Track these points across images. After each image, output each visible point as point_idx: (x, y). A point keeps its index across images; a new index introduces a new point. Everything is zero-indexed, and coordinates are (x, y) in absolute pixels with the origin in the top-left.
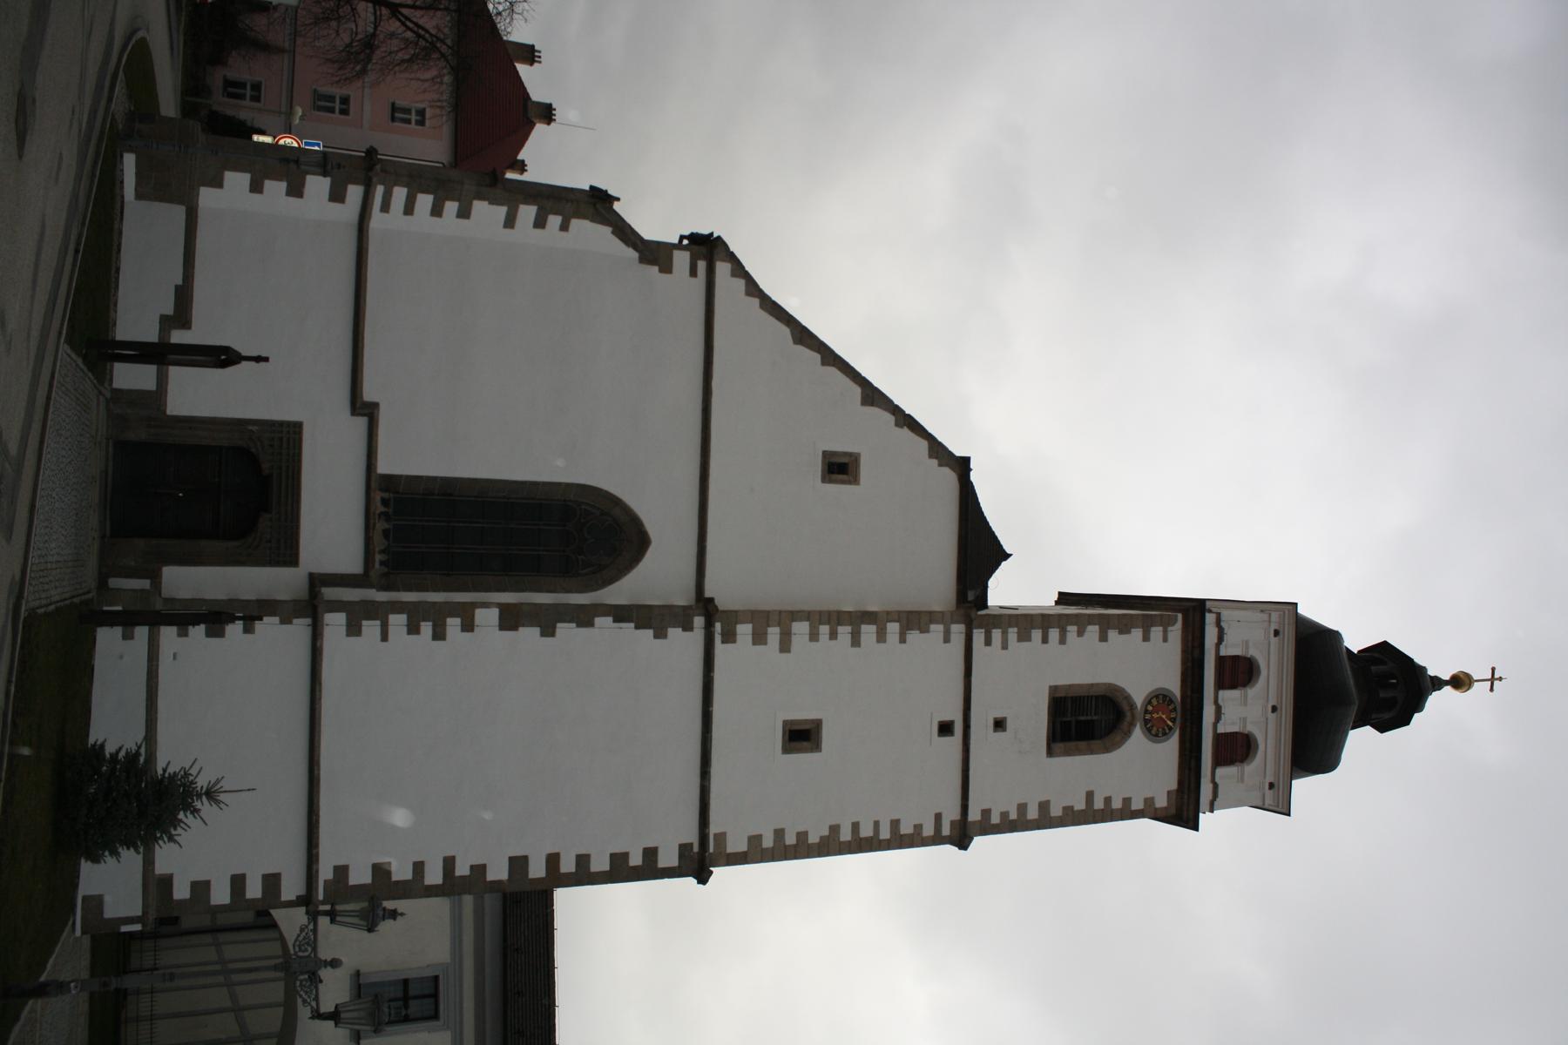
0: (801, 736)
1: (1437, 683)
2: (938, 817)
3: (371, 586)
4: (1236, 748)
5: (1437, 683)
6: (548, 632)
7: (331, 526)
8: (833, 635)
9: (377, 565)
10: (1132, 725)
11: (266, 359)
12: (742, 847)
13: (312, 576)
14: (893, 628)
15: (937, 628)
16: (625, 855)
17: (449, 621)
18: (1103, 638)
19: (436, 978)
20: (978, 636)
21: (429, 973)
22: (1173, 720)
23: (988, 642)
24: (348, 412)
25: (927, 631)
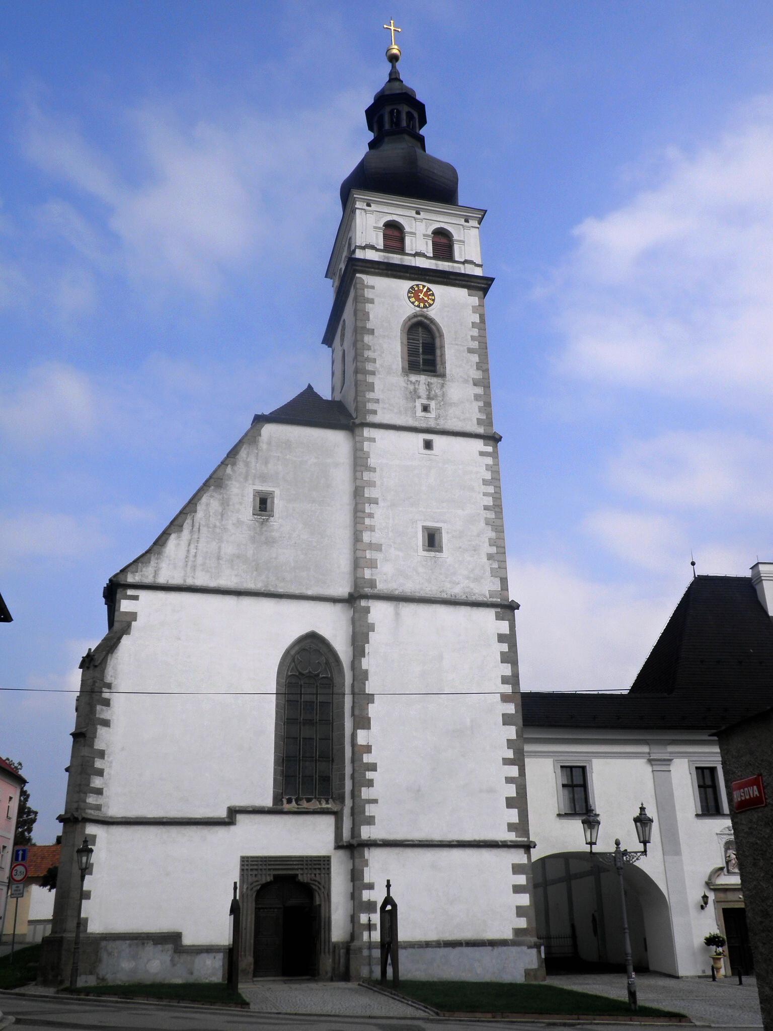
0: (432, 540)
1: (394, 77)
2: (482, 454)
3: (342, 810)
4: (443, 244)
5: (394, 77)
6: (370, 698)
7: (306, 837)
8: (371, 516)
9: (329, 806)
10: (426, 317)
11: (388, 881)
12: (498, 581)
13: (338, 847)
14: (366, 476)
16: (502, 653)
17: (365, 760)
19: (562, 767)
20: (371, 419)
21: (559, 770)
22: (424, 286)
24: (232, 828)
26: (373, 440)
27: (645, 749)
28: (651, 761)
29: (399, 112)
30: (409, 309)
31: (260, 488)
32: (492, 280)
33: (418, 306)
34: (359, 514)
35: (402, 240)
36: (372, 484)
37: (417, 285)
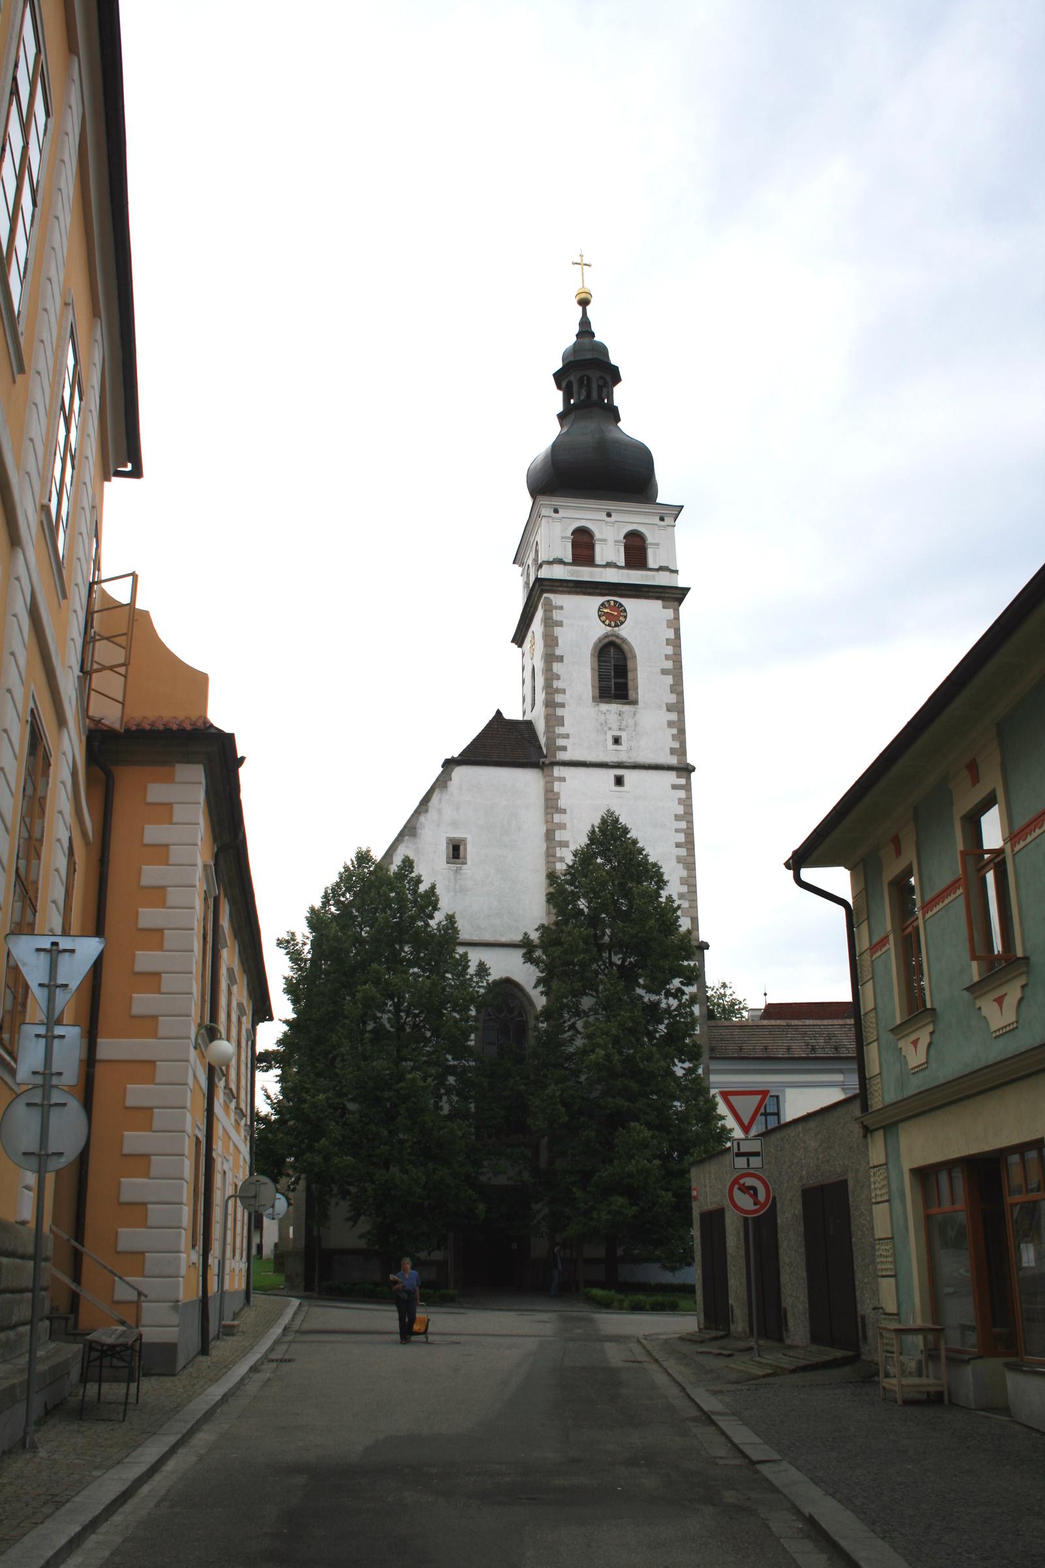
1: (585, 330)
2: (675, 787)
5: (585, 330)
10: (618, 637)
15: (557, 786)
18: (560, 659)
20: (562, 756)
23: (564, 749)
25: (558, 793)
26: (563, 779)
27: (839, 1077)
29: (589, 379)
30: (599, 630)
32: (688, 589)
33: (609, 625)
35: (592, 547)
36: (562, 826)
37: (608, 601)
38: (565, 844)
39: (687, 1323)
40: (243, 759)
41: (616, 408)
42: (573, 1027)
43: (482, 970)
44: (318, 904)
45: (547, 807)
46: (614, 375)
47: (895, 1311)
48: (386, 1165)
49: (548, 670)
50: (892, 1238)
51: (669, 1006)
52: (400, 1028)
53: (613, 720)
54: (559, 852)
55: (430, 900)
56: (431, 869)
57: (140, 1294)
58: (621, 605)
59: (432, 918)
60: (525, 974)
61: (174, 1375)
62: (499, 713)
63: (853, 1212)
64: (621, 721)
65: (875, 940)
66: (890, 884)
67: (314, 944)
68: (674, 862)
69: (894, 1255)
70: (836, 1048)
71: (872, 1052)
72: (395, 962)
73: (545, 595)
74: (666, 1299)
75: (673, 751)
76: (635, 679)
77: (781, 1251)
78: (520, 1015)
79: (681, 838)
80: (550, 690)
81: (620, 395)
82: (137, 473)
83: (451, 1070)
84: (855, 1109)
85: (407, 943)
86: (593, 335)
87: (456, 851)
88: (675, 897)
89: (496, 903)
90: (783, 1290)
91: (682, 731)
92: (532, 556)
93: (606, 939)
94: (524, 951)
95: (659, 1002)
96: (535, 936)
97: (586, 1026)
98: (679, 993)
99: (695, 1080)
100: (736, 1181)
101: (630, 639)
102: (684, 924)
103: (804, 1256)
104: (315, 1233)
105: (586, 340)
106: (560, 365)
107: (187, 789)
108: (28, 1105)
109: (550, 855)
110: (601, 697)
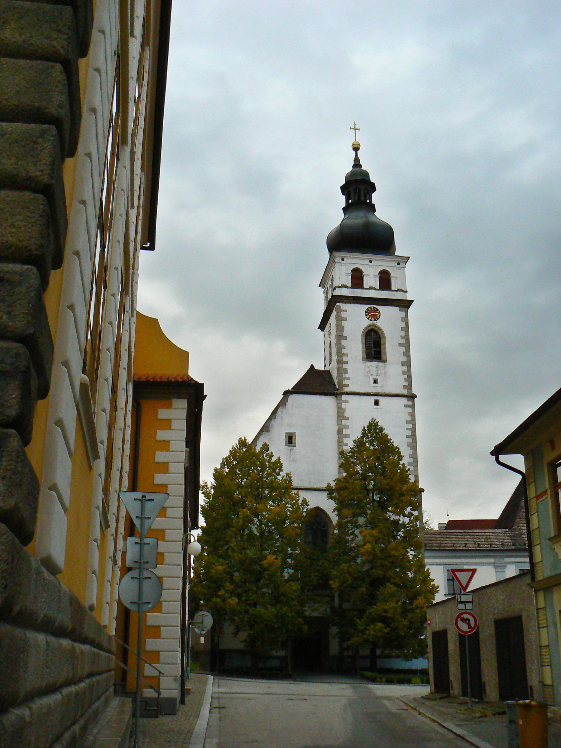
1: (357, 164)
2: (406, 406)
4: (385, 280)
5: (357, 164)
10: (375, 326)
15: (344, 406)
18: (345, 338)
20: (346, 389)
23: (348, 385)
25: (345, 409)
26: (347, 402)
27: (492, 560)
28: (495, 567)
29: (359, 190)
30: (366, 323)
31: (288, 431)
32: (413, 301)
33: (371, 320)
34: (341, 444)
35: (361, 279)
36: (347, 427)
37: (371, 307)
38: (348, 436)
39: (426, 690)
40: (206, 396)
41: (374, 205)
42: (353, 533)
43: (305, 502)
44: (219, 467)
45: (338, 416)
46: (372, 188)
47: (551, 684)
48: (255, 605)
49: (339, 344)
50: (548, 646)
51: (404, 522)
52: (262, 534)
53: (373, 370)
54: (345, 440)
55: (278, 465)
56: (278, 449)
57: (160, 673)
58: (377, 310)
59: (279, 474)
60: (328, 506)
61: (175, 714)
62: (312, 366)
63: (526, 633)
64: (377, 371)
65: (539, 493)
66: (548, 464)
67: (215, 488)
68: (406, 446)
69: (550, 654)
70: (491, 545)
71: (537, 550)
72: (259, 498)
73: (337, 304)
74: (404, 677)
75: (405, 387)
76: (385, 349)
77: (482, 652)
78: (324, 526)
79: (409, 433)
80: (339, 355)
81: (376, 198)
82: (152, 248)
83: (290, 556)
84: (528, 579)
85: (266, 488)
86: (361, 166)
87: (290, 439)
88: (406, 464)
89: (312, 467)
90: (482, 672)
91: (410, 376)
92: (330, 283)
93: (371, 486)
94: (328, 493)
95: (399, 520)
96: (333, 484)
97: (361, 532)
98: (409, 515)
99: (418, 560)
100: (459, 616)
101: (382, 328)
102: (412, 479)
103: (496, 656)
104: (216, 640)
105: (357, 169)
106: (344, 183)
107: (177, 412)
108: (132, 578)
109: (340, 442)
110: (367, 358)
